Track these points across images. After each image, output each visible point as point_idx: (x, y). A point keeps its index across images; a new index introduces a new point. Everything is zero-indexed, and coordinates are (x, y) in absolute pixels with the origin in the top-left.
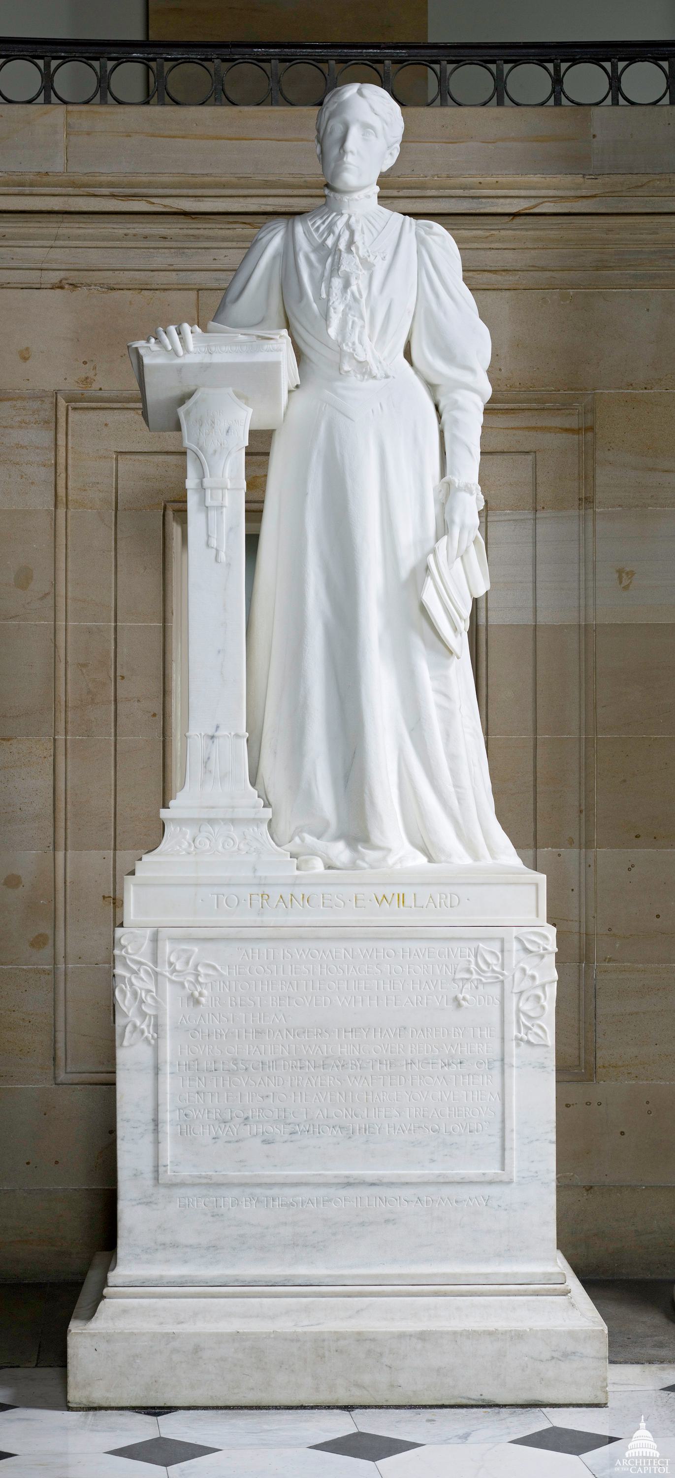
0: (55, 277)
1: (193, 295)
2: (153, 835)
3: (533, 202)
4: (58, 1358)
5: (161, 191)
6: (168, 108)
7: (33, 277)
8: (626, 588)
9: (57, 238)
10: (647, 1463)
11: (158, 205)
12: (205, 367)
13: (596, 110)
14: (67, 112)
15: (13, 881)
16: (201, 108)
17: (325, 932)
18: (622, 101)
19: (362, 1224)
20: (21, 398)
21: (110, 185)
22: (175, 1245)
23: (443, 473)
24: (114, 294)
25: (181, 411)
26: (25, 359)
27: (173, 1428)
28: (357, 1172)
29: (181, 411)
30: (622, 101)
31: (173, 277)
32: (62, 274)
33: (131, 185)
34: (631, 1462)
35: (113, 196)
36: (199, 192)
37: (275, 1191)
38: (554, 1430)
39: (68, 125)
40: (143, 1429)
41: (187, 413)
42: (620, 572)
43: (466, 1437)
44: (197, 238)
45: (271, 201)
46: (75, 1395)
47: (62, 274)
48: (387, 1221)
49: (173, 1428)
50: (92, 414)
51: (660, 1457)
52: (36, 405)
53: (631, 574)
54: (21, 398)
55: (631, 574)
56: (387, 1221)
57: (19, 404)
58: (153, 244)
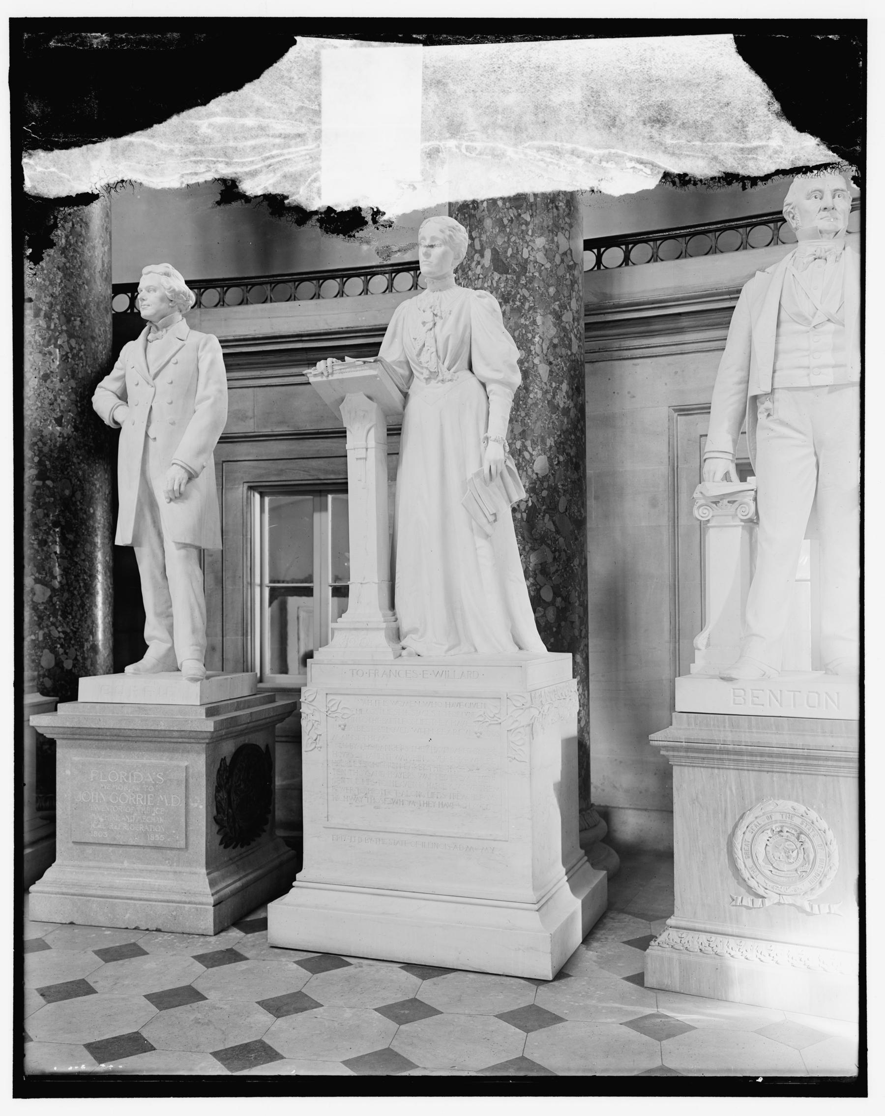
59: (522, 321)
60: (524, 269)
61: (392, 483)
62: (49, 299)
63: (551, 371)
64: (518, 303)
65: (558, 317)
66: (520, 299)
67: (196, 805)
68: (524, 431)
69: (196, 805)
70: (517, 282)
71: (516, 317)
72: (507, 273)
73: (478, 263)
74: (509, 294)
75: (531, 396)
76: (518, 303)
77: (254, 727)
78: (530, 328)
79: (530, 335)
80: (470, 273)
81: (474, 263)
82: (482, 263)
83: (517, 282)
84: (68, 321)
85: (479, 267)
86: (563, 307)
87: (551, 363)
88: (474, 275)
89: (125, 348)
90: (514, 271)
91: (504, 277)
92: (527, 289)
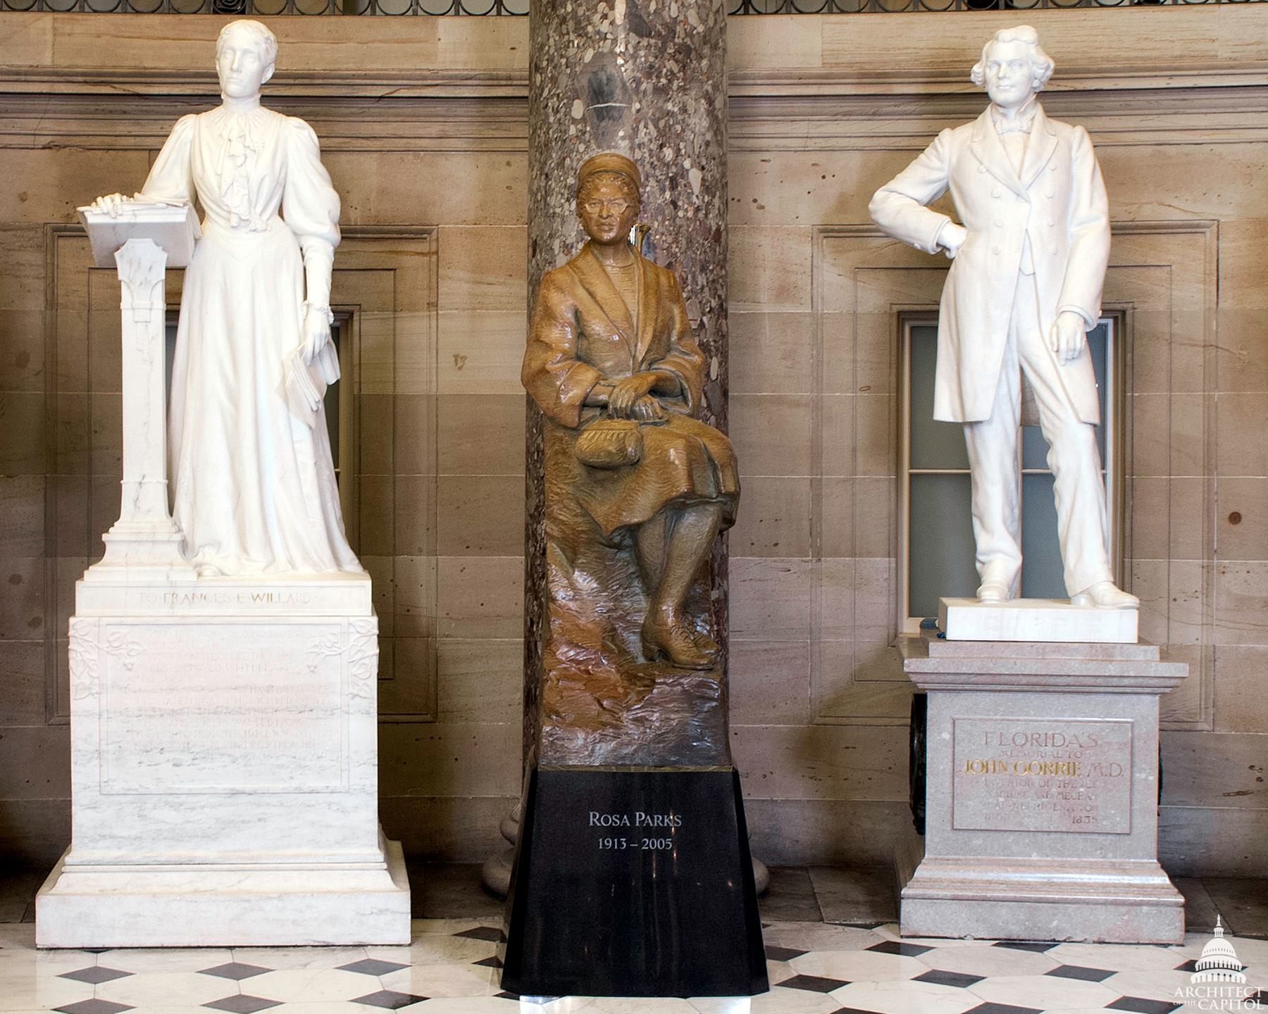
0: (44, 141)
1: (146, 154)
2: (95, 552)
3: (393, 89)
4: (29, 915)
5: (121, 79)
6: (128, 17)
7: (28, 140)
8: (460, 368)
9: (45, 112)
10: (1226, 991)
11: (119, 90)
12: (132, 226)
13: (441, 20)
14: (55, 19)
15: (15, 579)
16: (152, 16)
17: (216, 620)
18: (462, 12)
19: (243, 822)
20: (21, 229)
21: (83, 74)
22: (113, 837)
23: (305, 298)
24: (90, 153)
25: (117, 254)
26: (23, 200)
27: (104, 961)
28: (239, 786)
29: (117, 254)
30: (462, 12)
31: (131, 141)
32: (50, 139)
33: (99, 75)
34: (1201, 992)
35: (86, 82)
36: (149, 80)
37: (183, 798)
38: (369, 961)
39: (54, 29)
40: (86, 961)
41: (122, 256)
42: (456, 357)
43: (305, 965)
44: (148, 112)
45: (202, 87)
46: (41, 941)
47: (50, 139)
48: (260, 820)
49: (104, 961)
50: (72, 241)
51: (1247, 985)
52: (31, 234)
53: (464, 358)
54: (21, 229)
55: (464, 358)
56: (260, 820)
57: (19, 233)
58: (117, 117)
59: (670, 106)
60: (672, 32)
61: (172, 323)
63: (703, 179)
64: (663, 81)
65: (711, 102)
66: (666, 76)
67: (1143, 776)
68: (670, 263)
69: (1143, 776)
70: (662, 50)
71: (661, 101)
72: (649, 36)
73: (605, 16)
74: (651, 67)
75: (681, 214)
76: (663, 81)
77: (967, 863)
78: (680, 117)
79: (678, 128)
80: (590, 29)
81: (598, 16)
82: (610, 18)
83: (662, 50)
85: (606, 22)
86: (716, 87)
87: (703, 168)
88: (598, 32)
89: (80, 626)
90: (659, 34)
91: (644, 42)
92: (677, 61)
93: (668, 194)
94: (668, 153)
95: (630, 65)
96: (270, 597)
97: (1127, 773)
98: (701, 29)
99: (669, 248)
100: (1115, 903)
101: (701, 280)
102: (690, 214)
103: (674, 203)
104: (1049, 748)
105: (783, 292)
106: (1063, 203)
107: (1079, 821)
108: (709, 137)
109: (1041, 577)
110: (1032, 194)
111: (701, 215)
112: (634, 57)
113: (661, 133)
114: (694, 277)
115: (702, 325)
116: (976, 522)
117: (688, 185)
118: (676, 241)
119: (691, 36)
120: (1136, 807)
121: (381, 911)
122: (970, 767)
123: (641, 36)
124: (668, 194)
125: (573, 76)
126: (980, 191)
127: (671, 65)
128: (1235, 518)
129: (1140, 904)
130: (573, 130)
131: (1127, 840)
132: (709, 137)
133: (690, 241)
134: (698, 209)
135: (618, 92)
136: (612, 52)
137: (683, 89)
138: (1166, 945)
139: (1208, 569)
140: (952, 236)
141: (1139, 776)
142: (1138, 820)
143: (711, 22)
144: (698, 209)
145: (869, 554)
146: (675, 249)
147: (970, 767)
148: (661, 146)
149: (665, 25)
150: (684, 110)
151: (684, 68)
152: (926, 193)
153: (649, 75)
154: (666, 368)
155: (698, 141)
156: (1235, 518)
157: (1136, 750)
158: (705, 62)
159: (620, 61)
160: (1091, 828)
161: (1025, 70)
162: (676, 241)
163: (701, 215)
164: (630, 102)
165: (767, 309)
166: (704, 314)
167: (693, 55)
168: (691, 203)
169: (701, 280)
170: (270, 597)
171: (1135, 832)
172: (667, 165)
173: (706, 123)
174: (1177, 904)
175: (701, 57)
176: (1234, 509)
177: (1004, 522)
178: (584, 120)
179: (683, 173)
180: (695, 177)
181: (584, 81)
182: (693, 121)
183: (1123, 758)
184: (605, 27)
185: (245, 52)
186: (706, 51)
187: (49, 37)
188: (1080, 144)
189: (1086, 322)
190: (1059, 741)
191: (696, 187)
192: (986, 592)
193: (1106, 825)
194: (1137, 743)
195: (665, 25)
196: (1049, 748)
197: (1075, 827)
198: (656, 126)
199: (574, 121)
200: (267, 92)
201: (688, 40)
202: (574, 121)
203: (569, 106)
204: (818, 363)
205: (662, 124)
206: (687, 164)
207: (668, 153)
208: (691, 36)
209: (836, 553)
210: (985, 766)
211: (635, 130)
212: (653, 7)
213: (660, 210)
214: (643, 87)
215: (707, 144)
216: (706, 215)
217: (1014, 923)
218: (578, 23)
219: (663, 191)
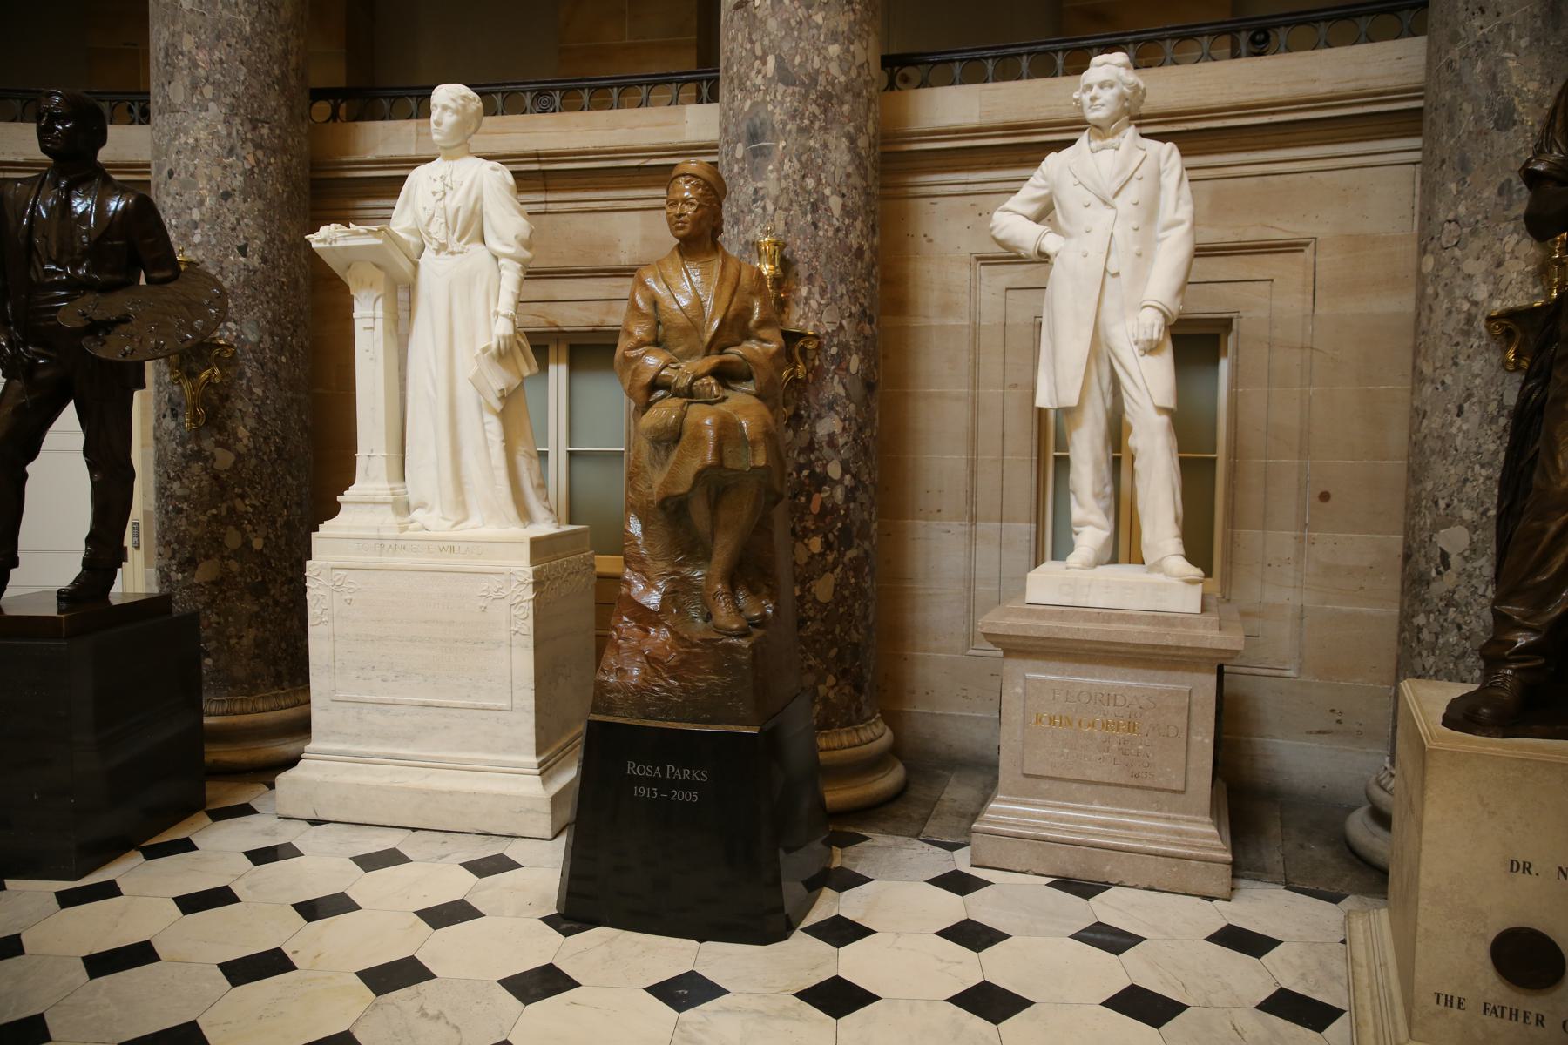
28: (429, 700)
59: (812, 143)
60: (814, 79)
62: (229, 100)
64: (806, 122)
67: (1199, 738)
69: (1199, 738)
70: (806, 96)
72: (794, 84)
73: (759, 72)
75: (821, 233)
76: (806, 122)
83: (806, 96)
84: (254, 128)
86: (859, 129)
90: (803, 83)
91: (790, 90)
93: (809, 217)
94: (810, 183)
95: (777, 111)
96: (452, 549)
97: (1183, 736)
98: (843, 79)
99: (809, 263)
100: (1165, 855)
101: (841, 289)
102: (830, 234)
103: (815, 225)
104: (1111, 708)
105: (946, 309)
106: (1150, 209)
107: (1137, 776)
108: (850, 169)
109: (1124, 545)
110: (1118, 201)
111: (841, 235)
112: (782, 103)
113: (804, 166)
114: (833, 287)
115: (841, 327)
116: (1072, 497)
117: (829, 209)
118: (816, 256)
119: (833, 85)
120: (1191, 766)
121: (528, 811)
122: (1038, 720)
123: (787, 85)
124: (809, 217)
125: (737, 125)
126: (1071, 198)
127: (813, 108)
128: (1325, 497)
129: (1190, 858)
130: (736, 169)
131: (1182, 797)
132: (850, 169)
133: (829, 257)
134: (838, 230)
135: (769, 133)
136: (764, 100)
137: (825, 129)
138: (1211, 899)
139: (1300, 540)
140: (1051, 243)
141: (1196, 738)
142: (1192, 778)
143: (854, 74)
144: (838, 230)
145: (1015, 520)
146: (815, 263)
147: (1038, 720)
148: (804, 177)
149: (808, 75)
150: (825, 146)
151: (825, 112)
152: (1032, 209)
153: (793, 117)
154: (735, 353)
155: (839, 172)
156: (1325, 497)
157: (1193, 714)
158: (846, 108)
159: (770, 107)
160: (1147, 782)
161: (1115, 91)
162: (816, 256)
163: (841, 235)
164: (777, 142)
165: (935, 322)
166: (843, 317)
167: (835, 101)
168: (831, 225)
169: (841, 289)
170: (452, 549)
171: (1190, 789)
172: (809, 193)
173: (847, 158)
174: (1225, 863)
175: (842, 103)
176: (1324, 489)
177: (1096, 496)
178: (743, 159)
179: (824, 199)
180: (835, 203)
181: (744, 127)
182: (834, 156)
183: (1181, 721)
184: (759, 80)
185: (445, 108)
186: (848, 97)
187: (414, 137)
188: (1169, 157)
189: (1165, 316)
190: (1120, 701)
191: (837, 211)
192: (1073, 559)
193: (1161, 782)
194: (1193, 708)
195: (808, 75)
196: (1111, 708)
197: (1133, 782)
198: (799, 160)
199: (737, 161)
200: (1178, 331)
201: (830, 88)
202: (737, 161)
203: (734, 149)
204: (975, 364)
205: (804, 158)
206: (827, 191)
207: (810, 183)
208: (833, 85)
209: (988, 519)
210: (1052, 720)
211: (782, 164)
212: (797, 60)
213: (802, 230)
214: (789, 127)
215: (849, 176)
216: (847, 236)
217: (1073, 867)
218: (740, 80)
219: (805, 214)
